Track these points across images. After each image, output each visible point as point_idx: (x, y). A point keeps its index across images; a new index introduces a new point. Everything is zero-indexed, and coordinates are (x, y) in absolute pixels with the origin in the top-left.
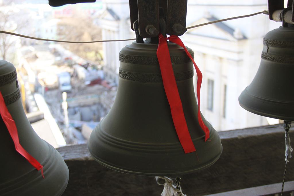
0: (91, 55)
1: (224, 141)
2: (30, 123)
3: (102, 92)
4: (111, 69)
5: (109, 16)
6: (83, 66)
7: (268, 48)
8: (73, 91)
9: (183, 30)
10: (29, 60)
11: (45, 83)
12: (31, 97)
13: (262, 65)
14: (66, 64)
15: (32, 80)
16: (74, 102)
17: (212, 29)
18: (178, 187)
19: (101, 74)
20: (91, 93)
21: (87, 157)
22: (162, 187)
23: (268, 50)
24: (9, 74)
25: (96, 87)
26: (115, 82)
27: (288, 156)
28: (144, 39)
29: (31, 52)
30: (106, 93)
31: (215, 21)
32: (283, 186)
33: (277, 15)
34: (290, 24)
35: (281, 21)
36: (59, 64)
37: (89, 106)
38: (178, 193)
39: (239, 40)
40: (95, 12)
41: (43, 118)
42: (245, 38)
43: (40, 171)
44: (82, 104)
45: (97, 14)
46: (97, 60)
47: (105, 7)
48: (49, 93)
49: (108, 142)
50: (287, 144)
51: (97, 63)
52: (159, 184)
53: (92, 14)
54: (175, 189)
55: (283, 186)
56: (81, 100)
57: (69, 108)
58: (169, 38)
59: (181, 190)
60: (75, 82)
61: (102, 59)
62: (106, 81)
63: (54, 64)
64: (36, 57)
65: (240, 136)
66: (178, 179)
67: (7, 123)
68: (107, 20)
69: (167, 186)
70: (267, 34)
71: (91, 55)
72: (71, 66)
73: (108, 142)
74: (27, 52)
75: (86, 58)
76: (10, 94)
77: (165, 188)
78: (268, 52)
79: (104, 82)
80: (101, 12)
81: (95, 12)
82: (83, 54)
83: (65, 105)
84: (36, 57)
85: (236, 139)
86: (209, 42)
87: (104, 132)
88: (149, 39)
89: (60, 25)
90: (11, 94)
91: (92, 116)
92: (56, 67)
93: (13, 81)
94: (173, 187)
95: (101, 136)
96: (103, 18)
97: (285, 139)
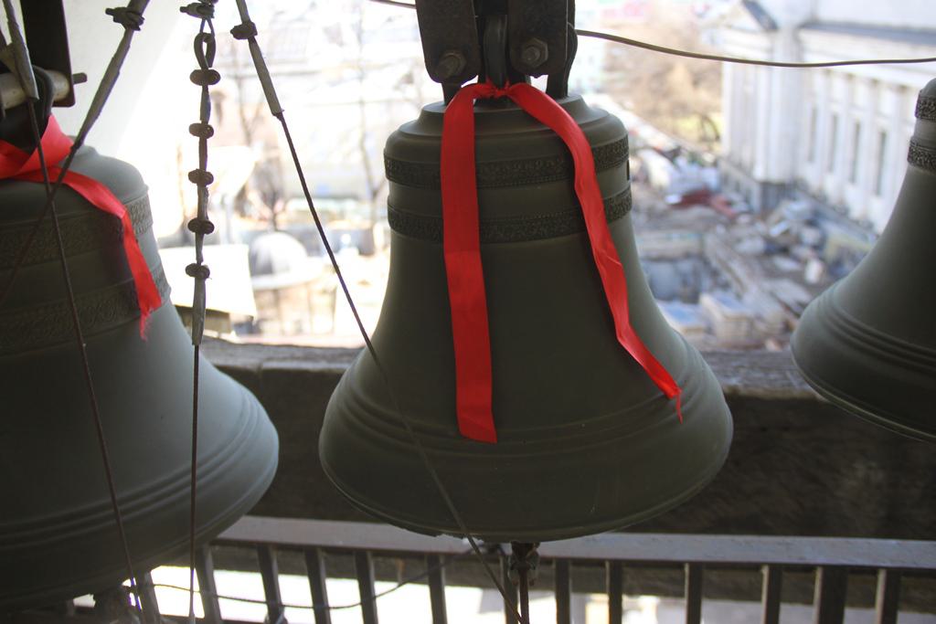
3: (709, 225)
4: (740, 166)
6: (662, 153)
19: (711, 177)
20: (680, 226)
21: (736, 386)
24: (612, 144)
25: (696, 211)
26: (747, 200)
30: (720, 230)
37: (671, 260)
40: (707, 8)
43: (673, 402)
44: (654, 254)
45: (713, 15)
46: (704, 139)
49: (862, 344)
51: (704, 147)
61: (718, 138)
62: (723, 197)
67: (602, 267)
68: (743, 30)
71: (689, 126)
73: (869, 347)
75: (674, 133)
76: (615, 195)
79: (717, 201)
80: (725, 8)
81: (707, 8)
82: (668, 121)
87: (843, 312)
90: (619, 195)
91: (679, 288)
93: (623, 161)
95: (842, 328)
96: (730, 27)
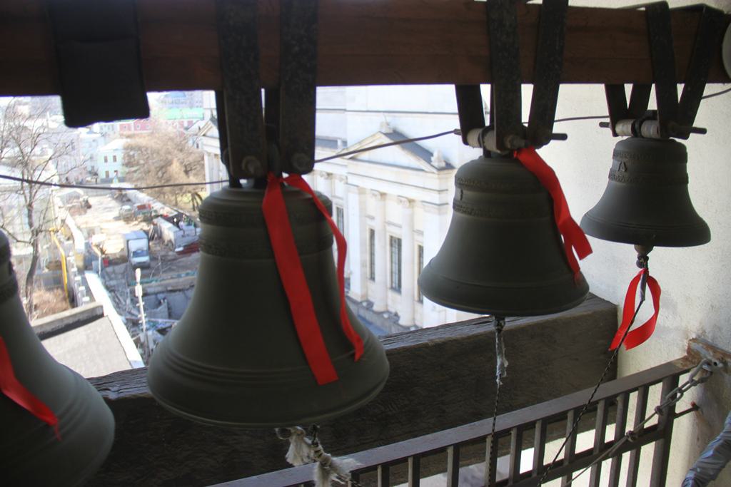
1: (390, 354)
2: (38, 339)
7: (462, 192)
8: (153, 264)
9: (309, 169)
10: (74, 211)
11: (103, 252)
12: (78, 278)
13: (455, 222)
14: (141, 216)
15: (80, 245)
16: (155, 286)
17: (397, 154)
18: (315, 441)
20: (185, 267)
22: (288, 444)
23: (462, 196)
27: (500, 375)
28: (243, 181)
29: (78, 197)
31: (400, 139)
32: (494, 425)
33: (474, 136)
34: (495, 153)
35: (480, 147)
36: (128, 218)
38: (316, 452)
39: (440, 169)
40: (191, 123)
41: (102, 316)
48: (109, 269)
50: (499, 354)
52: (281, 438)
53: (187, 129)
54: (309, 446)
55: (494, 425)
56: (169, 280)
57: (145, 295)
58: (286, 179)
59: (320, 447)
60: (157, 248)
63: (117, 219)
64: (88, 206)
65: (432, 340)
66: (315, 428)
69: (295, 441)
70: (465, 164)
72: (149, 220)
74: (69, 199)
77: (291, 445)
78: (463, 199)
81: (191, 123)
83: (139, 290)
84: (88, 206)
85: (426, 346)
86: (389, 173)
88: (252, 181)
89: (128, 148)
92: (122, 223)
94: (306, 443)
97: (497, 346)
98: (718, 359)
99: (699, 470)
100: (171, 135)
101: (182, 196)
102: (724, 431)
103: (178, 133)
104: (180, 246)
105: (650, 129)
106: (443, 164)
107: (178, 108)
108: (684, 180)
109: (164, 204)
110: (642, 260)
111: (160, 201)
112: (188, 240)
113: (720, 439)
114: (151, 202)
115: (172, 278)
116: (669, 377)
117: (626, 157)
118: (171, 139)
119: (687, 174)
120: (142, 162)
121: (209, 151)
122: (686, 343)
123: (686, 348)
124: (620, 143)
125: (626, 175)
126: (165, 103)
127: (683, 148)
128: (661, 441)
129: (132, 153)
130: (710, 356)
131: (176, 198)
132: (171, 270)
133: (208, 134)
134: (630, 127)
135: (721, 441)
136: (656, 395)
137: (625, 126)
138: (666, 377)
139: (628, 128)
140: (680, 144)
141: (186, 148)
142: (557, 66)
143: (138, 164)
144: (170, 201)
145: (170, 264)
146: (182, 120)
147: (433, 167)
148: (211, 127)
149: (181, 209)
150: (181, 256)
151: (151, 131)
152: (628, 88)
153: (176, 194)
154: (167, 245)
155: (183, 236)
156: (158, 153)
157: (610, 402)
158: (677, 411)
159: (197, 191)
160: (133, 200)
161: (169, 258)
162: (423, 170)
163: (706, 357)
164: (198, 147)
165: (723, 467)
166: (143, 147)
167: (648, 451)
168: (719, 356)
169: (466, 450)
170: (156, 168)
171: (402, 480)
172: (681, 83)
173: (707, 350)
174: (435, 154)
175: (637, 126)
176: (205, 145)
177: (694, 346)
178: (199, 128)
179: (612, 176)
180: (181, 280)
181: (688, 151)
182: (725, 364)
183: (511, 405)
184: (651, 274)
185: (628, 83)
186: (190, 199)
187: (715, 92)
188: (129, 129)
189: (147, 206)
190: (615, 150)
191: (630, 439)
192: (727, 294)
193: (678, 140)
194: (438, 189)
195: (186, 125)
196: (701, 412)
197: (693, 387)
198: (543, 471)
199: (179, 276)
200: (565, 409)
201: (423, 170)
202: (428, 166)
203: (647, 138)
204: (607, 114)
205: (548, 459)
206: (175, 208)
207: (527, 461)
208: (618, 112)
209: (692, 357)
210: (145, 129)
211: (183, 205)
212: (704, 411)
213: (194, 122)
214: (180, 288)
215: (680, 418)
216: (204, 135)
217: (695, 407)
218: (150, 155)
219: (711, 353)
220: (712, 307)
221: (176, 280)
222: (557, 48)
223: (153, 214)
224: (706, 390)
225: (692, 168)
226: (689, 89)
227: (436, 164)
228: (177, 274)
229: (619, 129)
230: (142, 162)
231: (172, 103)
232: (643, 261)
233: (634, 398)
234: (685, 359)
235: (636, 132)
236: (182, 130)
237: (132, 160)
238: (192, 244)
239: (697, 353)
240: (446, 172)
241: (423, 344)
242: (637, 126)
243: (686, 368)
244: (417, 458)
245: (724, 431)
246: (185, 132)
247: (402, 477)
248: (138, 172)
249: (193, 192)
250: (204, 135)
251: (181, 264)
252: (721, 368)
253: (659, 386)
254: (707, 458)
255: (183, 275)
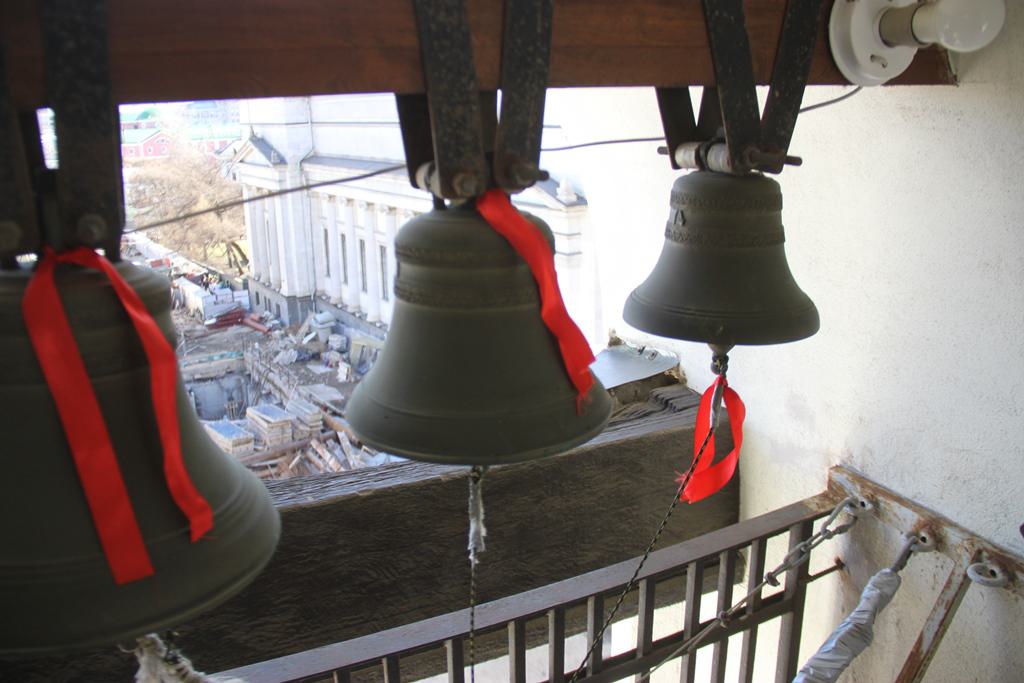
0: (218, 253)
5: (258, 156)
19: (243, 298)
20: (218, 347)
25: (233, 330)
26: (278, 316)
27: (475, 549)
42: (581, 201)
47: (247, 135)
50: (473, 514)
52: (124, 651)
53: (219, 152)
65: (447, 474)
78: (402, 277)
97: (470, 504)
98: (867, 497)
99: (812, 672)
100: (197, 162)
101: (213, 247)
102: (857, 609)
103: (205, 159)
104: (212, 317)
105: (719, 158)
106: (574, 198)
107: (206, 123)
108: (778, 237)
109: (188, 258)
110: (718, 363)
111: (183, 255)
112: (222, 309)
113: (849, 623)
114: (170, 257)
115: (200, 362)
116: (801, 525)
117: (684, 203)
118: (196, 167)
119: (782, 228)
120: (156, 200)
121: (250, 184)
122: (826, 471)
123: (827, 479)
124: (682, 180)
125: (685, 230)
126: (188, 116)
127: (775, 186)
128: (789, 616)
129: (141, 188)
130: (856, 492)
131: (205, 251)
132: (199, 350)
133: (248, 159)
134: (693, 154)
135: (850, 626)
136: (778, 550)
137: (688, 153)
138: (756, 539)
139: (690, 156)
140: (771, 180)
141: (217, 180)
142: (539, 61)
143: (150, 203)
144: (197, 254)
145: (199, 343)
146: (212, 140)
147: (559, 201)
148: (252, 150)
149: (212, 265)
150: (213, 331)
151: (168, 156)
152: (696, 94)
153: (206, 245)
154: (193, 316)
155: (215, 303)
156: (178, 187)
157: (735, 556)
158: (811, 572)
159: (234, 239)
160: (145, 253)
161: (197, 334)
162: (545, 207)
163: (851, 494)
164: (235, 178)
165: (847, 665)
166: (157, 179)
167: (770, 632)
168: (869, 492)
169: (526, 631)
170: (176, 208)
171: (577, 629)
172: (763, 84)
173: (854, 484)
174: (563, 185)
175: (702, 153)
176: (244, 175)
177: (839, 477)
178: (235, 152)
179: (668, 234)
180: (213, 364)
181: (783, 191)
182: (876, 504)
183: (575, 565)
184: (731, 385)
185: (760, 84)
186: (225, 250)
187: (830, 99)
188: (138, 154)
189: (164, 261)
190: (673, 192)
191: (722, 624)
192: (879, 401)
193: (767, 175)
194: (566, 232)
195: (217, 147)
196: (846, 572)
197: (826, 541)
198: (651, 652)
199: (211, 359)
200: (686, 561)
201: (545, 207)
202: (553, 201)
203: (716, 172)
204: (661, 133)
205: (659, 632)
206: (204, 264)
207: (576, 652)
208: (678, 130)
209: (833, 492)
210: (160, 154)
211: (214, 260)
212: (852, 572)
213: (228, 143)
214: (213, 375)
215: (815, 581)
216: (241, 161)
217: (839, 565)
218: (167, 189)
219: (859, 488)
220: (861, 419)
221: (206, 365)
222: (539, 30)
223: (173, 273)
224: (854, 539)
225: (789, 217)
226: (777, 94)
227: (563, 198)
228: (207, 355)
229: (680, 156)
230: (156, 200)
231: (198, 116)
232: (721, 363)
233: (749, 553)
234: (824, 496)
235: (701, 161)
236: (212, 154)
237: (143, 197)
238: (228, 314)
239: (841, 488)
240: (577, 208)
241: (433, 480)
242: (702, 153)
243: (822, 510)
244: (600, 598)
245: (857, 609)
246: (217, 157)
247: (409, 674)
248: (151, 214)
249: (228, 240)
250: (241, 161)
251: (213, 342)
252: (870, 511)
253: (786, 537)
254: (829, 652)
255: (216, 358)
